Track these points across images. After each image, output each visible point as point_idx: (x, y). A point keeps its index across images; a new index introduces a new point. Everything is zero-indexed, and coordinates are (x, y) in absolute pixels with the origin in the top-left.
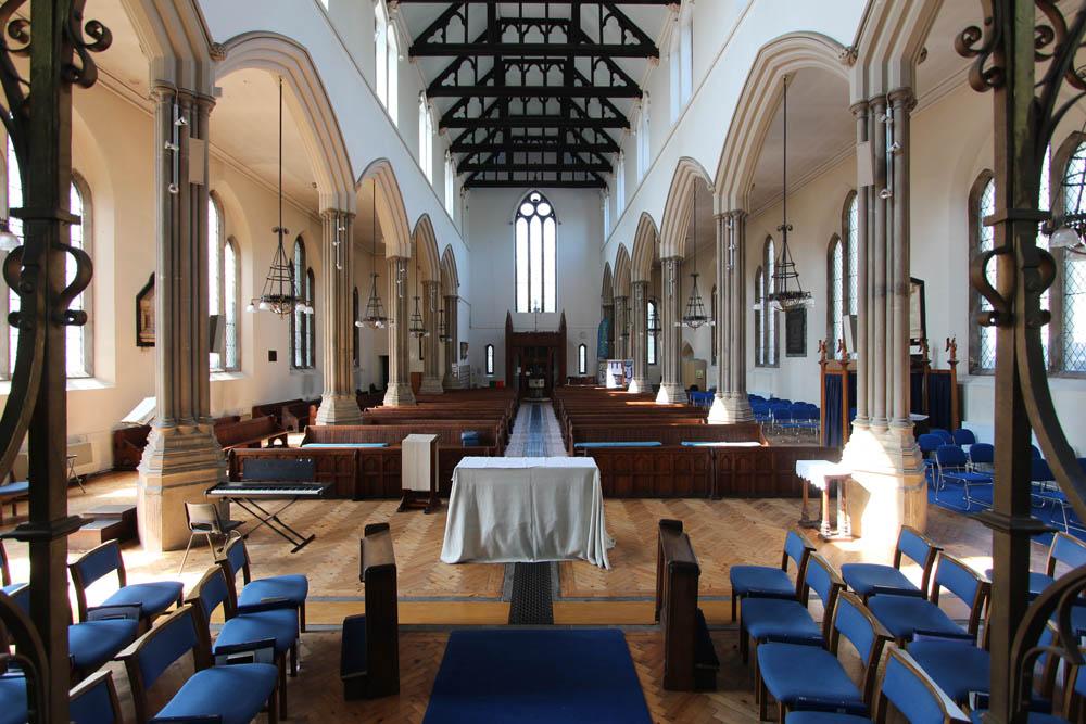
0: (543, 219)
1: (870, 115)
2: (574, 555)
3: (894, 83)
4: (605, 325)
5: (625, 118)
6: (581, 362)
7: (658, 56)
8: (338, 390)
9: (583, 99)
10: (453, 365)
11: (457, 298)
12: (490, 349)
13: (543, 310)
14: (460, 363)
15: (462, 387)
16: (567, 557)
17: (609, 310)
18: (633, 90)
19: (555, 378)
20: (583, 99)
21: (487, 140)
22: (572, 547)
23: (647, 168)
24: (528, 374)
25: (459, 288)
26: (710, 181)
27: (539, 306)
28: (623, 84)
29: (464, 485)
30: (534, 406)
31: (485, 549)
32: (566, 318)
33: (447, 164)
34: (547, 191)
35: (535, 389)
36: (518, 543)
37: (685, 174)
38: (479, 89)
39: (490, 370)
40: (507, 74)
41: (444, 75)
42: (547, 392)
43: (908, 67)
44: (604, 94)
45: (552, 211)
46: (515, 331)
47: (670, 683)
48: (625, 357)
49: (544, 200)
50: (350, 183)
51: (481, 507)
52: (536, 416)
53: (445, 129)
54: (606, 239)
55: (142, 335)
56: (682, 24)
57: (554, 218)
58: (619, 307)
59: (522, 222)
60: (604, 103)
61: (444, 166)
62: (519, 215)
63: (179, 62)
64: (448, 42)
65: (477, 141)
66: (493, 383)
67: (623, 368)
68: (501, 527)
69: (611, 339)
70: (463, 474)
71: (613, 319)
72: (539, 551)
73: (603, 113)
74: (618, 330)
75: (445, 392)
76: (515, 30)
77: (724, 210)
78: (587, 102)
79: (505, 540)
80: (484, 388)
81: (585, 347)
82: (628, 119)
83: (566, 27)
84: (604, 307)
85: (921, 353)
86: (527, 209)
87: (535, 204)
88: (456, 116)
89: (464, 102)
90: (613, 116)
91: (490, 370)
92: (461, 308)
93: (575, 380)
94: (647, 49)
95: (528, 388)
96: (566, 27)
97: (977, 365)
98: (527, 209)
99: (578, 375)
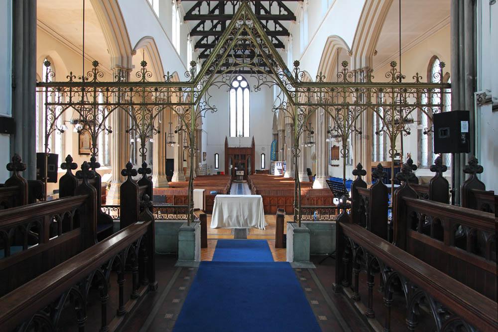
0: (243, 89)
1: (357, 75)
2: (254, 227)
3: (363, 65)
4: (274, 143)
5: (282, 43)
6: (262, 163)
7: (295, 20)
8: (159, 174)
9: (265, 21)
10: (200, 164)
11: (201, 130)
12: (217, 155)
13: (243, 136)
14: (203, 163)
15: (204, 175)
16: (252, 227)
17: (276, 135)
18: (285, 33)
19: (249, 171)
20: (265, 21)
21: (212, 29)
22: (253, 224)
23: (306, 44)
24: (236, 168)
25: (202, 126)
26: (349, 48)
27: (241, 134)
28: (281, 29)
29: (218, 203)
30: (239, 184)
31: (225, 223)
32: (255, 139)
33: (188, 42)
34: (245, 75)
35: (239, 176)
36: (236, 222)
37: (332, 46)
38: (211, 16)
39: (217, 167)
40: (226, 6)
41: (193, 9)
42: (245, 177)
43: (369, 59)
44: (276, 19)
45: (248, 85)
46: (229, 146)
47: (277, 246)
48: (283, 160)
49: (244, 79)
50: (128, 48)
51: (224, 210)
52: (240, 188)
53: (197, 49)
54: (274, 100)
55: (80, 150)
56: (305, 10)
57: (249, 88)
58: (280, 135)
59: (233, 91)
60: (276, 23)
61: (187, 43)
62: (231, 87)
63: (122, 57)
64: (201, 14)
65: (209, 42)
66: (219, 173)
67: (282, 165)
68: (230, 217)
69: (277, 151)
70: (218, 199)
71: (278, 141)
72: (242, 225)
73: (280, 11)
74: (280, 147)
75: (197, 177)
76: (231, 3)
77: (358, 67)
78: (271, 5)
79: (231, 221)
80: (214, 175)
81: (264, 154)
82: (284, 44)
83: (254, 2)
84: (274, 135)
85: (400, 159)
86: (235, 84)
87: (240, 82)
88: (193, 13)
89: (203, 22)
90: (281, 29)
91: (217, 167)
92: (203, 135)
93: (258, 172)
94: (291, 17)
95: (236, 176)
96: (254, 2)
97: (420, 164)
98: (235, 84)
99: (260, 169)
